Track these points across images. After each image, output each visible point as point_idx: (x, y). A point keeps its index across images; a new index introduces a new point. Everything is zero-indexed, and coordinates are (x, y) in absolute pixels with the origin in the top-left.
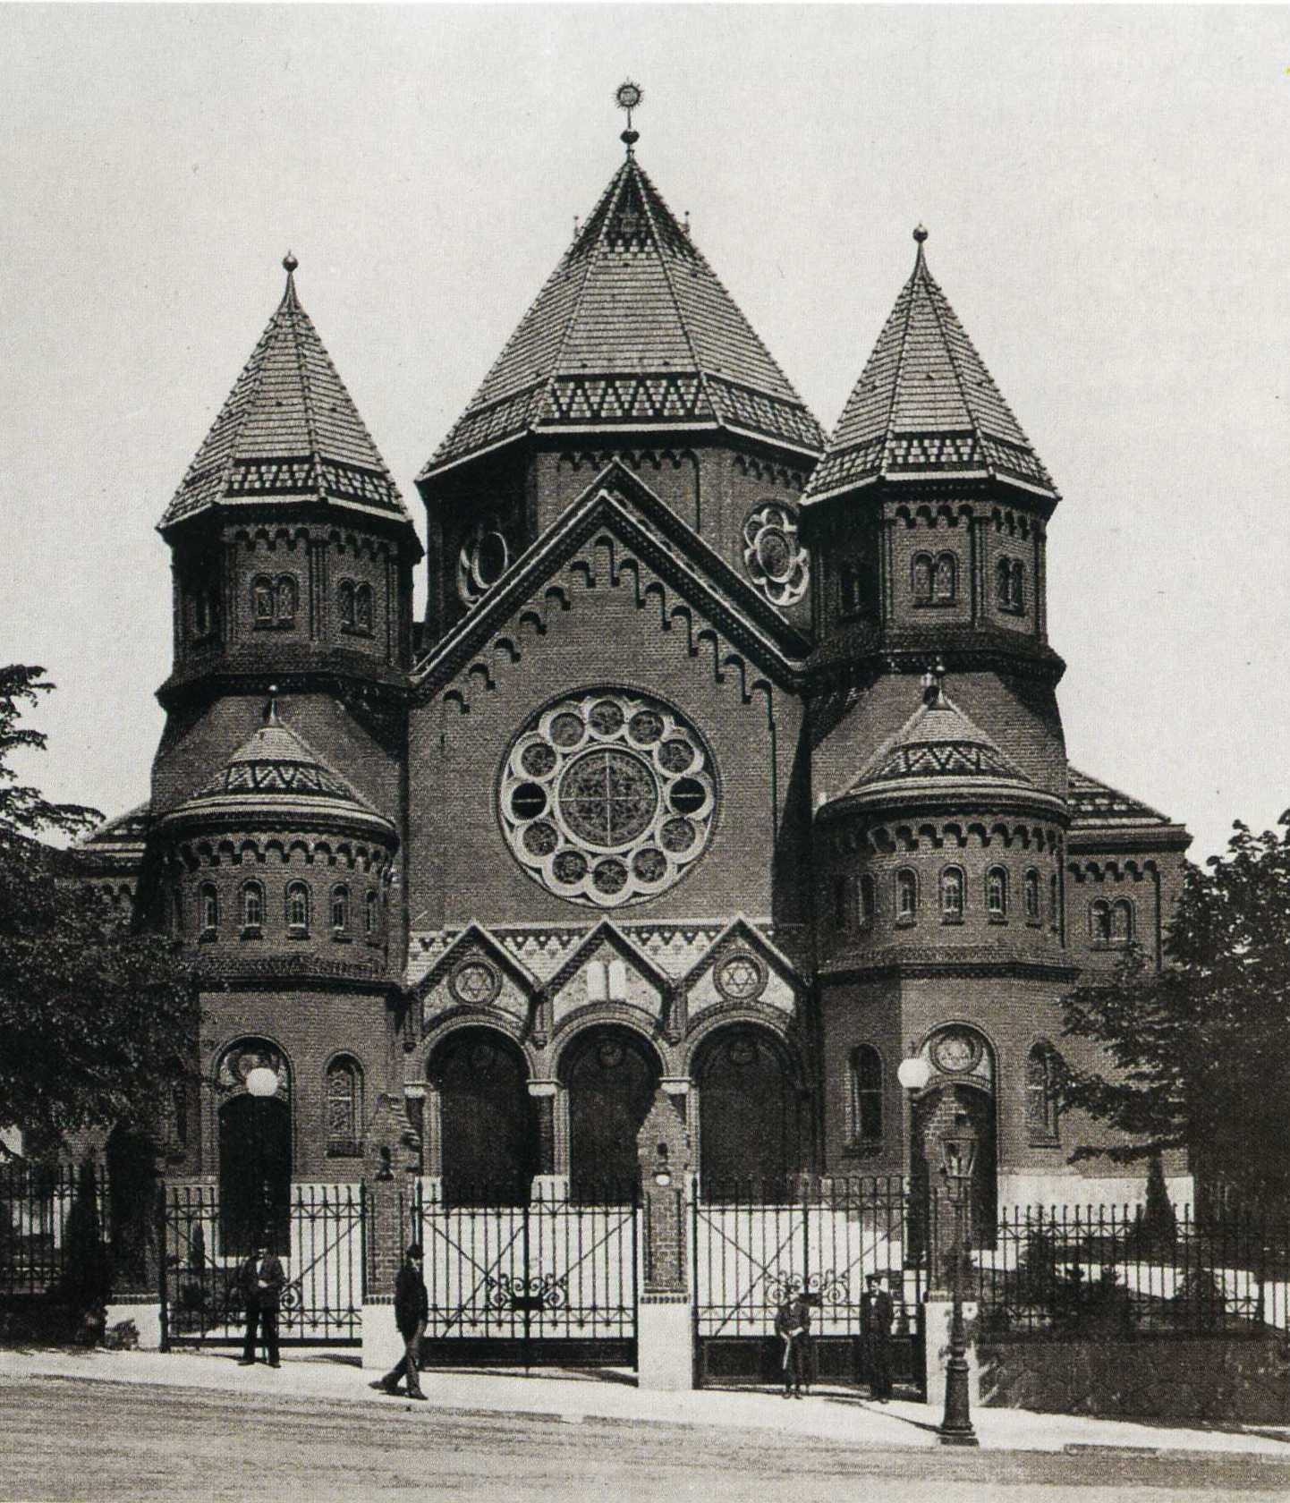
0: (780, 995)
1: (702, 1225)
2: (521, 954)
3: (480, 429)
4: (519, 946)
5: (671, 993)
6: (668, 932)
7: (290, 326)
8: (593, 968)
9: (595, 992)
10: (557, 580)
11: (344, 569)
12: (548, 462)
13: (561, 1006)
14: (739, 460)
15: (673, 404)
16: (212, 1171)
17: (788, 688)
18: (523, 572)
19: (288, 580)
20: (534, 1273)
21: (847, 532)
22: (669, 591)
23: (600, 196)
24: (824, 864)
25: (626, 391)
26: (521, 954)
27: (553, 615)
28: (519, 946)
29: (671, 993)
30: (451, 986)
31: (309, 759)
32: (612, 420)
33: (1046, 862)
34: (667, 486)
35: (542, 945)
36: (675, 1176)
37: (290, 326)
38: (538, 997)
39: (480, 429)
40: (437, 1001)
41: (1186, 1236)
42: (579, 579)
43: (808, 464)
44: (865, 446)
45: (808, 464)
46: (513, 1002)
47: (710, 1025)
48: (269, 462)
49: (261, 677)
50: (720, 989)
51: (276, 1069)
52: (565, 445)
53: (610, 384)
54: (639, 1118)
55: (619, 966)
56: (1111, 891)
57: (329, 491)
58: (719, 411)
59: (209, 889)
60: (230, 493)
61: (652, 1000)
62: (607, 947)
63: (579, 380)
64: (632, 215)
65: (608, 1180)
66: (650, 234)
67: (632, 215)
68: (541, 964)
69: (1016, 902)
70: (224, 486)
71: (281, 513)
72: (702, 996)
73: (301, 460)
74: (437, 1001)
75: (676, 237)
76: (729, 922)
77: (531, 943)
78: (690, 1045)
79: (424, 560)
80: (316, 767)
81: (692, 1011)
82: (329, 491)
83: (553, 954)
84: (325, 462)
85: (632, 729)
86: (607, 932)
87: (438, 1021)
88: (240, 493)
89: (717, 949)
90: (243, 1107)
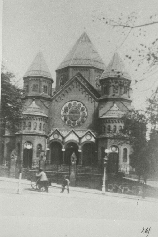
8: (71, 135)
10: (70, 87)
11: (44, 84)
12: (93, 70)
14: (95, 70)
17: (97, 101)
18: (59, 92)
19: (37, 85)
21: (105, 82)
22: (83, 89)
24: (99, 125)
27: (59, 100)
32: (79, 65)
34: (84, 74)
38: (64, 138)
41: (142, 180)
42: (72, 87)
43: (103, 71)
44: (108, 73)
45: (103, 71)
46: (60, 138)
49: (13, 109)
51: (31, 145)
55: (74, 135)
64: (85, 38)
67: (85, 38)
68: (64, 134)
72: (84, 140)
75: (90, 41)
77: (64, 131)
85: (67, 119)
86: (73, 131)
90: (26, 150)
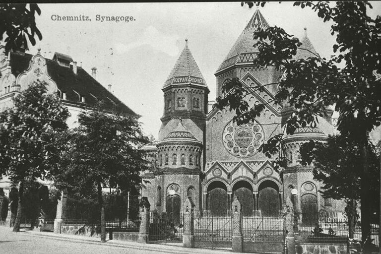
1: (244, 221)
2: (227, 167)
4: (226, 165)
6: (254, 163)
7: (187, 54)
8: (240, 169)
9: (240, 174)
13: (233, 177)
20: (214, 229)
23: (252, 17)
26: (227, 167)
28: (226, 165)
29: (255, 175)
30: (213, 173)
31: (186, 131)
35: (230, 165)
38: (229, 175)
40: (210, 176)
46: (224, 176)
47: (262, 181)
48: (181, 77)
50: (213, 174)
52: (241, 67)
53: (245, 55)
55: (245, 169)
57: (191, 82)
59: (291, 153)
60: (174, 83)
61: (251, 176)
62: (242, 166)
63: (245, 54)
66: (260, 24)
70: (173, 82)
71: (182, 86)
73: (187, 77)
74: (210, 176)
76: (240, 161)
78: (232, 185)
80: (188, 133)
81: (208, 179)
82: (191, 82)
83: (232, 167)
84: (191, 77)
87: (210, 180)
88: (176, 83)
89: (264, 165)
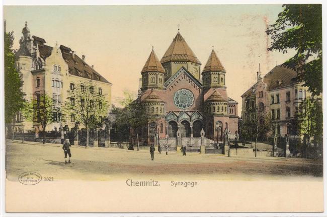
0: (201, 117)
3: (165, 59)
5: (178, 117)
7: (213, 54)
8: (184, 115)
12: (172, 63)
13: (180, 119)
15: (185, 58)
16: (104, 141)
25: (180, 56)
29: (191, 117)
33: (226, 106)
36: (203, 137)
37: (213, 54)
38: (178, 117)
39: (165, 59)
54: (201, 131)
55: (186, 115)
56: (231, 108)
58: (191, 58)
64: (178, 38)
65: (197, 135)
67: (178, 38)
69: (224, 109)
79: (201, 73)
